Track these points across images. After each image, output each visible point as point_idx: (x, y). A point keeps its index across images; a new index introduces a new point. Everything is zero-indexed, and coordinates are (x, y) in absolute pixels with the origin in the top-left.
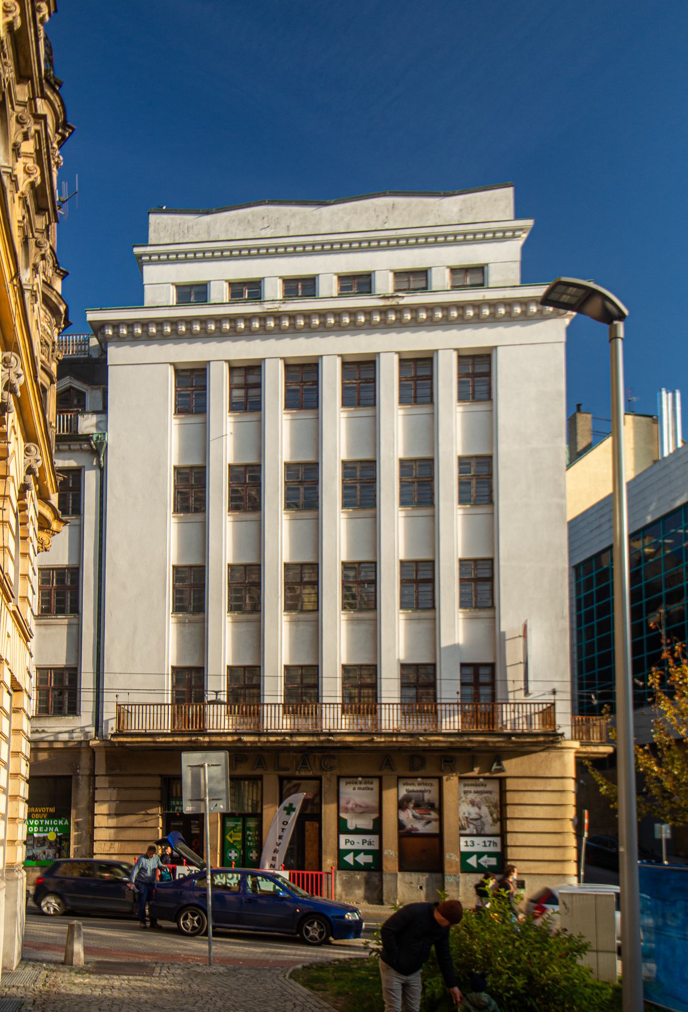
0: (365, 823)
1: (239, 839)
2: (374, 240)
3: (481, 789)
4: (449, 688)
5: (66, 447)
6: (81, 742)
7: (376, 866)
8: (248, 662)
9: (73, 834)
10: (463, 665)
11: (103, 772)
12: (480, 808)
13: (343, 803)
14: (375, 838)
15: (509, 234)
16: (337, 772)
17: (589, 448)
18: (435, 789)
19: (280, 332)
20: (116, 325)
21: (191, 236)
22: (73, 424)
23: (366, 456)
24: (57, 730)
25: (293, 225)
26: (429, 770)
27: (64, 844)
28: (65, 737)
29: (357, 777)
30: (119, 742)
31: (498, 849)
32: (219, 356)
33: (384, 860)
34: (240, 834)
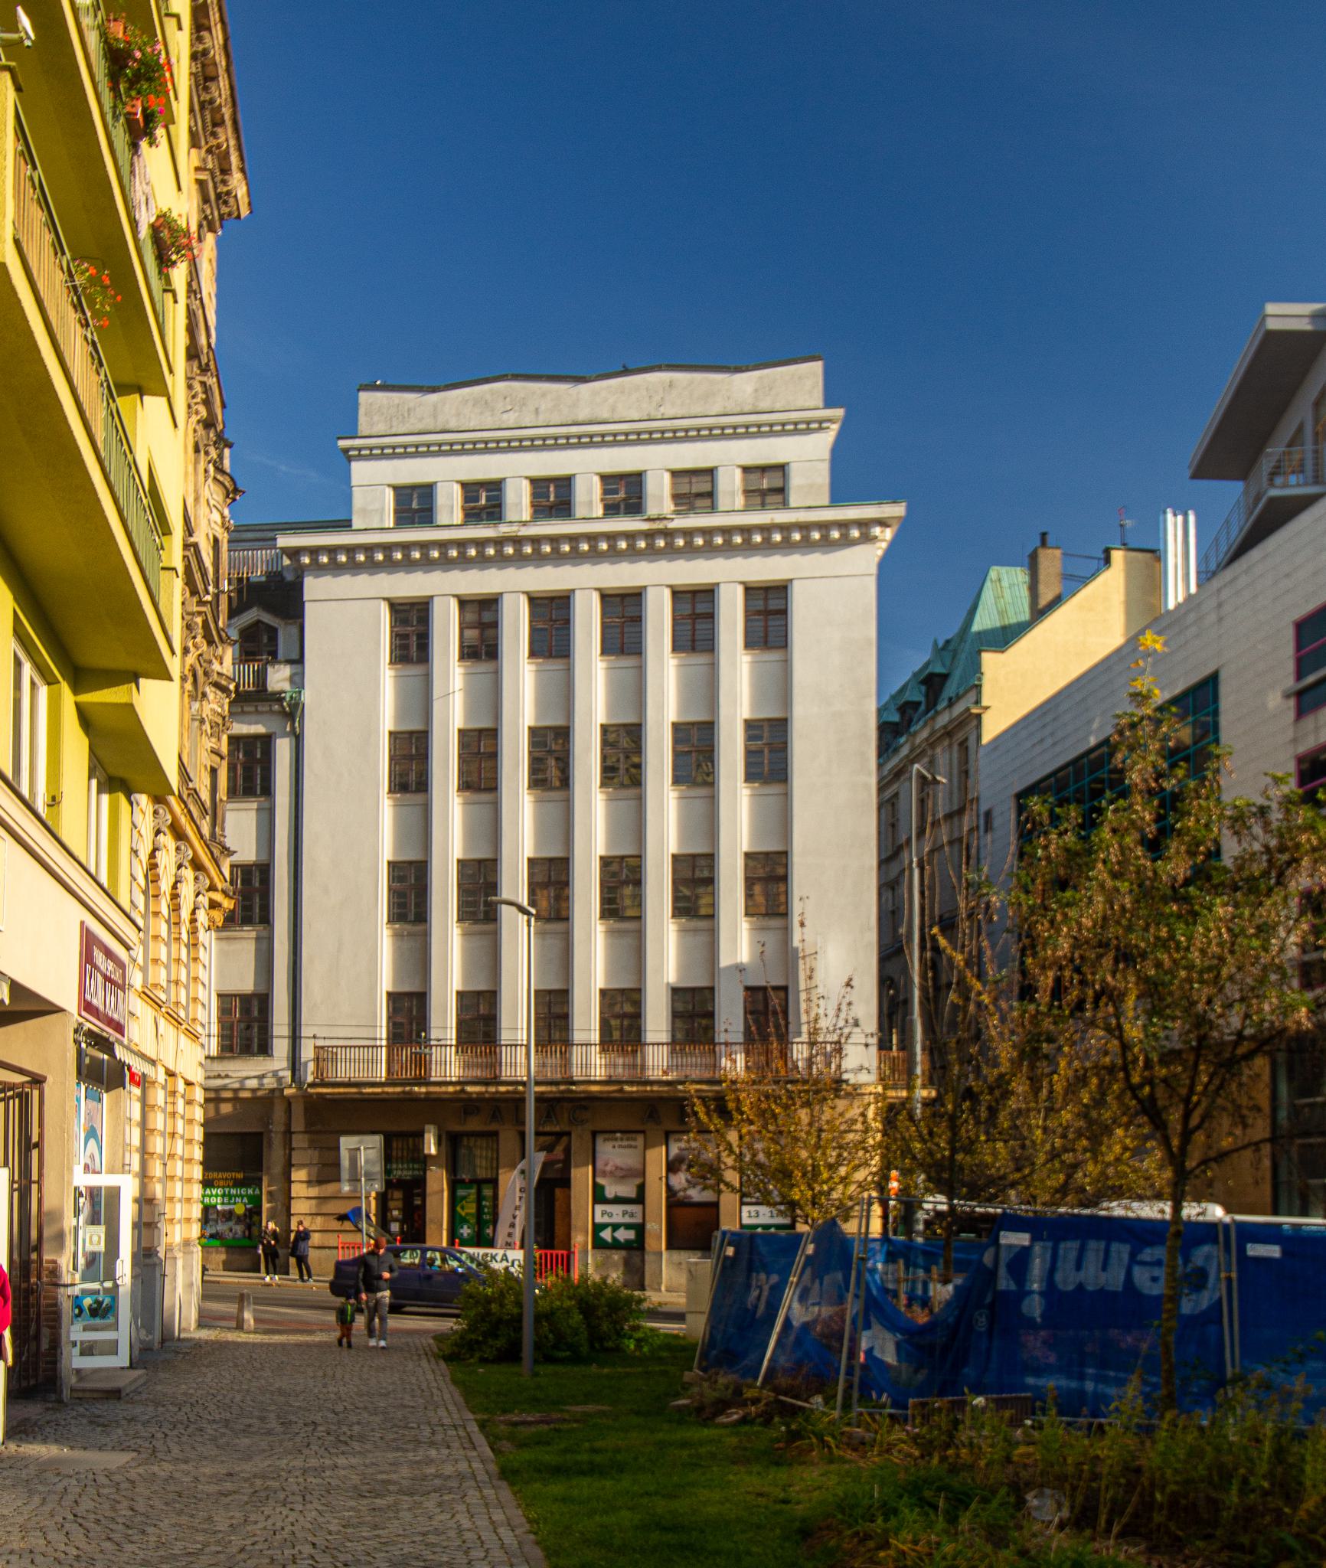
0: (628, 1190)
1: (473, 1211)
2: (645, 432)
4: (730, 1017)
5: (252, 709)
6: (272, 1091)
7: (637, 1246)
8: (482, 987)
9: (266, 1206)
10: (747, 989)
11: (302, 1129)
13: (599, 1164)
14: (636, 1209)
15: (814, 426)
16: (590, 1127)
17: (1057, 602)
19: (520, 560)
20: (314, 551)
21: (412, 420)
22: (261, 678)
23: (630, 719)
24: (244, 1074)
25: (543, 408)
27: (255, 1218)
28: (253, 1083)
29: (615, 1132)
30: (318, 1094)
32: (444, 590)
33: (647, 1235)
34: (474, 1205)
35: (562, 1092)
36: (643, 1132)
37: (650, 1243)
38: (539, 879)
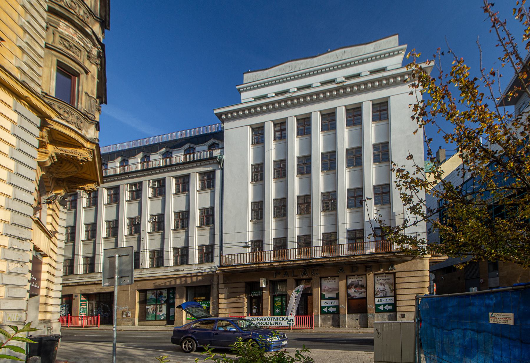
0: (333, 295)
3: (385, 278)
6: (213, 272)
7: (337, 313)
9: (211, 306)
13: (323, 288)
14: (336, 301)
15: (396, 53)
18: (364, 279)
20: (226, 113)
26: (360, 272)
28: (208, 270)
31: (393, 302)
35: (307, 263)
36: (338, 276)
37: (341, 311)
38: (301, 202)
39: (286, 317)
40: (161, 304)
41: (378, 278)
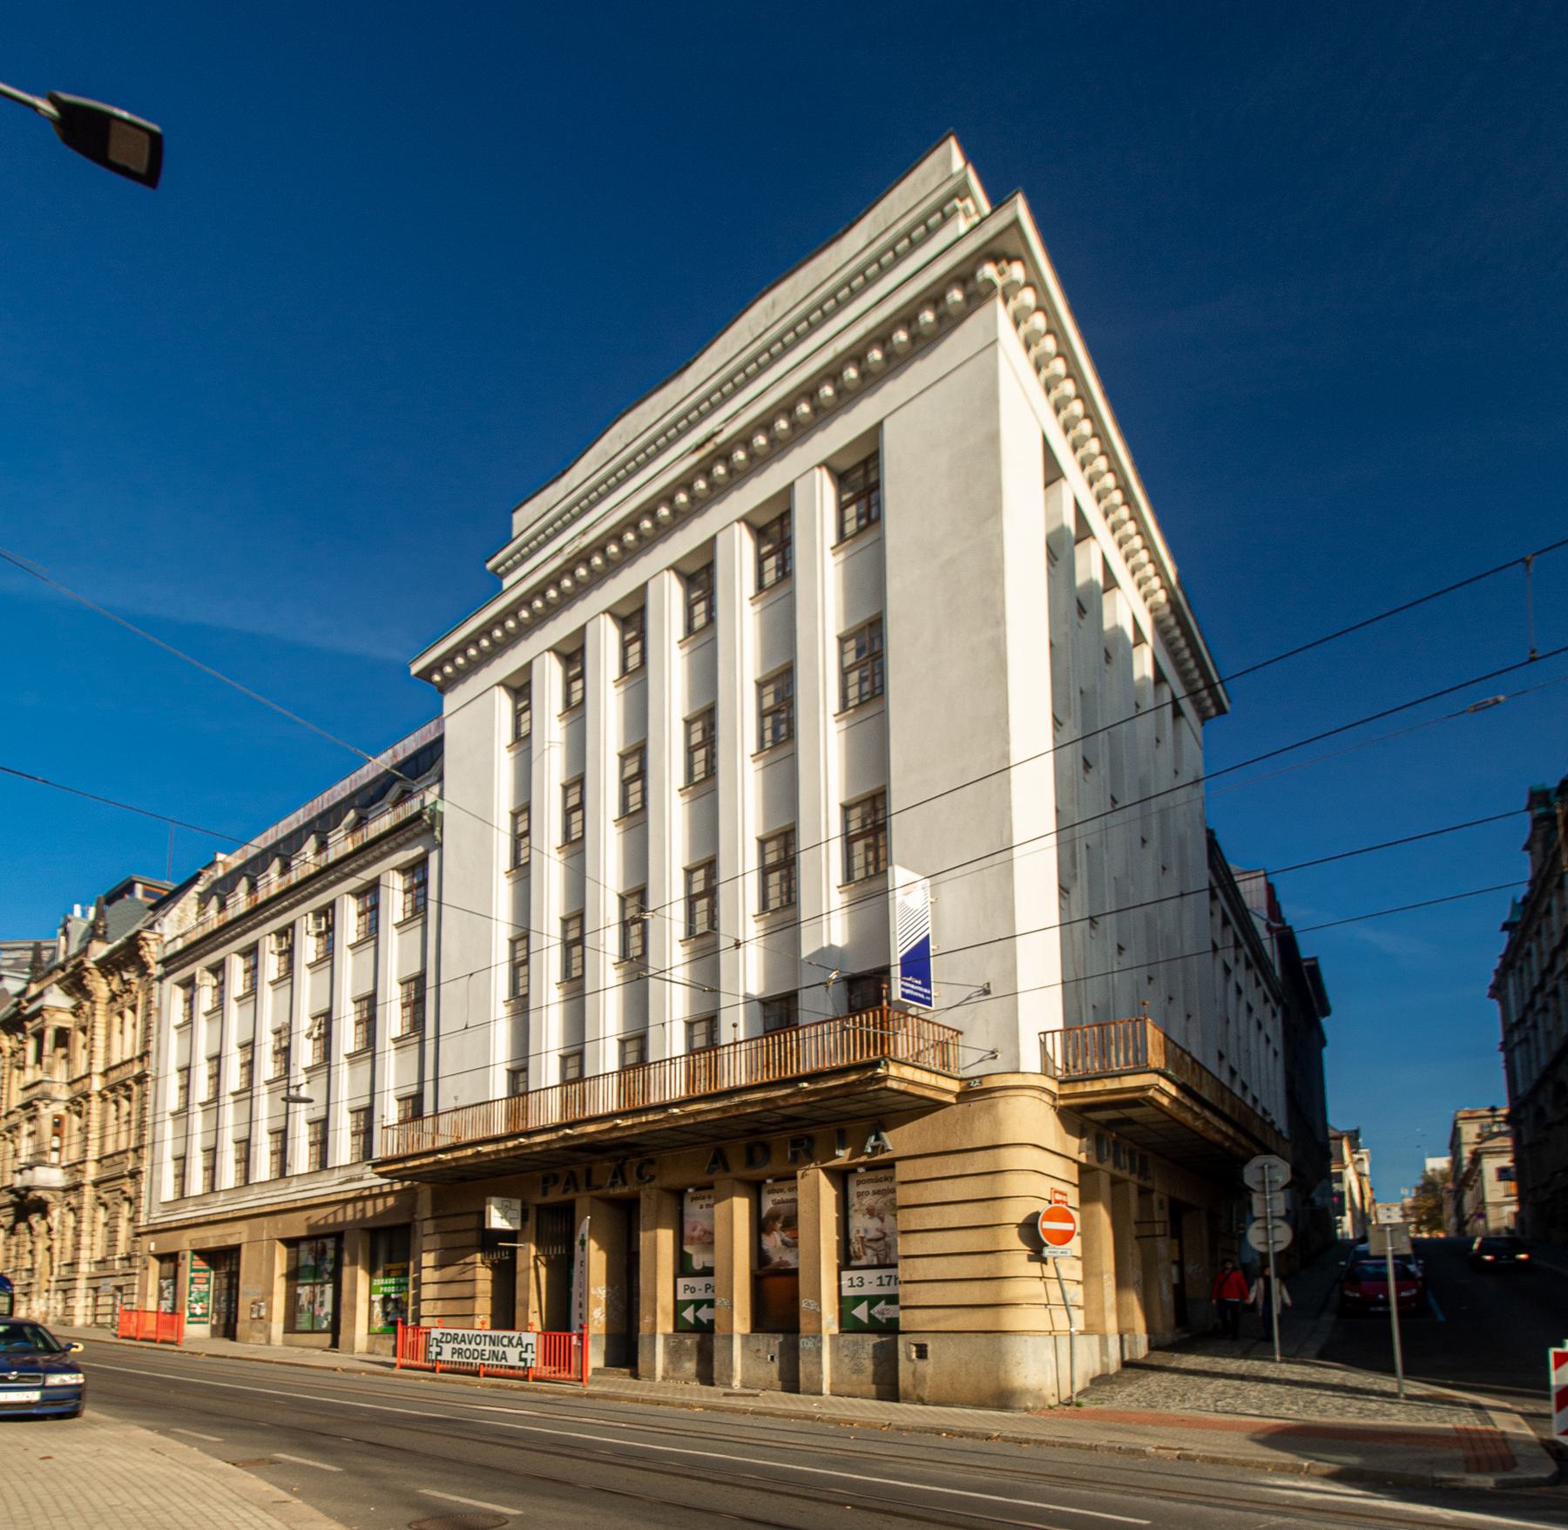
12: (882, 1220)
13: (687, 1230)
39: (516, 1334)
40: (322, 1284)
41: (862, 1188)
